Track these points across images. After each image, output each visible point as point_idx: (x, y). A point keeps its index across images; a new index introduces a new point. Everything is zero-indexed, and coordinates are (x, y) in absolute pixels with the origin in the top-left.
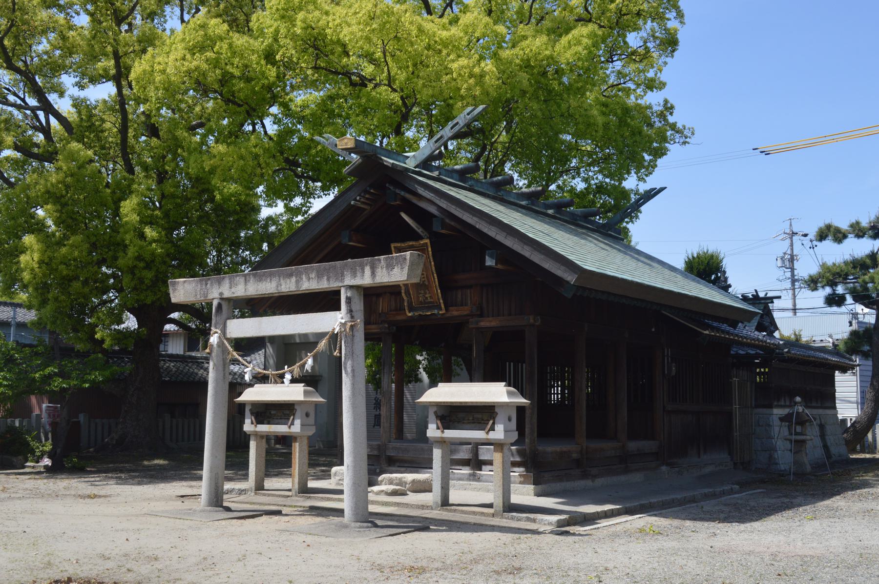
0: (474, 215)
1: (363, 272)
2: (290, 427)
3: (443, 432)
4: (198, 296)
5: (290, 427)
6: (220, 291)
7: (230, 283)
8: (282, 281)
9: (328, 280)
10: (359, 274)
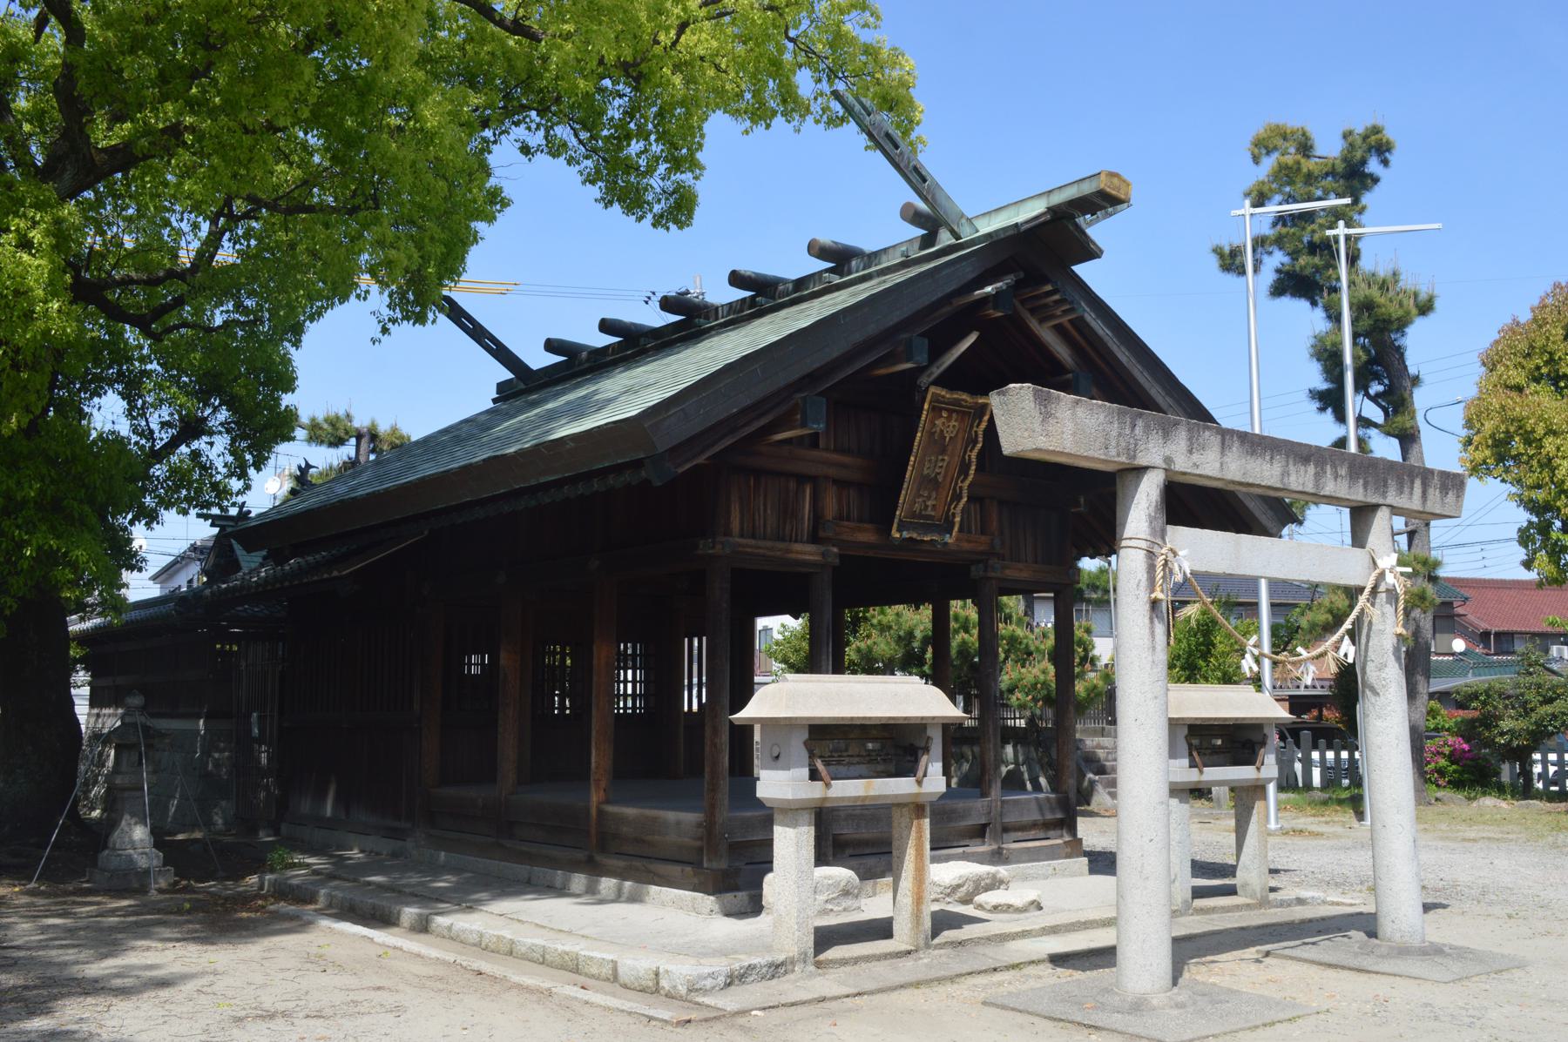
0: (1169, 393)
1: (1412, 489)
2: (919, 783)
3: (1201, 772)
4: (1113, 452)
5: (919, 783)
7: (1190, 439)
8: (1291, 467)
10: (1406, 490)
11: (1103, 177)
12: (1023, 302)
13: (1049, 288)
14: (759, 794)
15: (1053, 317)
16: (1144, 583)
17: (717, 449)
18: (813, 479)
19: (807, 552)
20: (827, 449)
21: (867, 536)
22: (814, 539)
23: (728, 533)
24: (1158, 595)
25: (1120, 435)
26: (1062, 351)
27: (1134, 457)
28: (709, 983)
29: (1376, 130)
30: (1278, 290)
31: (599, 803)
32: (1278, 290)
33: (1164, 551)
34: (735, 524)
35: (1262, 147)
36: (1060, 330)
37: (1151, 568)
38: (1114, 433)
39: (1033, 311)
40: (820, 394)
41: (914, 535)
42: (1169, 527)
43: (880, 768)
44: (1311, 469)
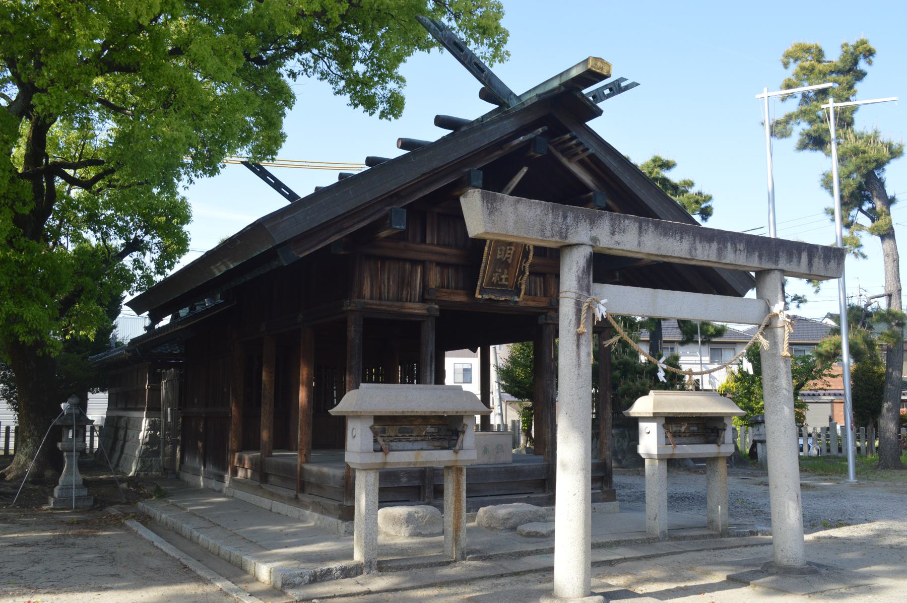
1: (800, 258)
4: (548, 234)
6: (594, 234)
7: (612, 225)
9: (760, 257)
10: (795, 259)
11: (590, 61)
12: (556, 147)
13: (568, 136)
14: (346, 460)
15: (577, 154)
16: (573, 321)
17: (328, 242)
18: (423, 263)
19: (416, 308)
20: (432, 244)
21: (460, 298)
22: (423, 300)
23: (360, 296)
24: (582, 329)
25: (553, 223)
26: (586, 178)
27: (566, 237)
28: (298, 580)
29: (863, 42)
30: (803, 146)
31: (302, 463)
32: (803, 146)
33: (588, 300)
34: (367, 291)
35: (790, 57)
36: (582, 163)
37: (578, 312)
38: (549, 221)
39: (563, 152)
40: (403, 207)
41: (493, 297)
42: (597, 288)
43: (437, 444)
44: (715, 246)
